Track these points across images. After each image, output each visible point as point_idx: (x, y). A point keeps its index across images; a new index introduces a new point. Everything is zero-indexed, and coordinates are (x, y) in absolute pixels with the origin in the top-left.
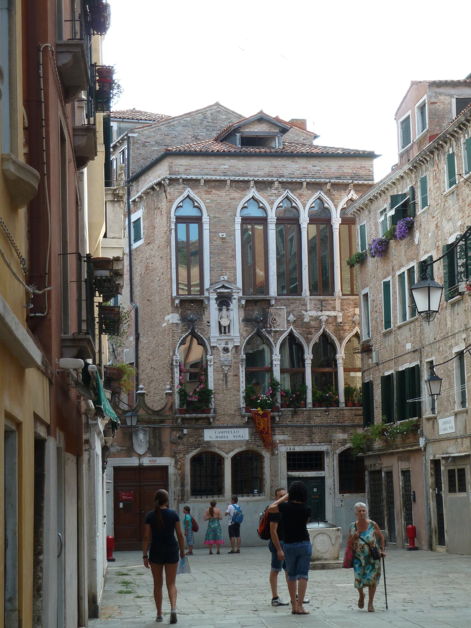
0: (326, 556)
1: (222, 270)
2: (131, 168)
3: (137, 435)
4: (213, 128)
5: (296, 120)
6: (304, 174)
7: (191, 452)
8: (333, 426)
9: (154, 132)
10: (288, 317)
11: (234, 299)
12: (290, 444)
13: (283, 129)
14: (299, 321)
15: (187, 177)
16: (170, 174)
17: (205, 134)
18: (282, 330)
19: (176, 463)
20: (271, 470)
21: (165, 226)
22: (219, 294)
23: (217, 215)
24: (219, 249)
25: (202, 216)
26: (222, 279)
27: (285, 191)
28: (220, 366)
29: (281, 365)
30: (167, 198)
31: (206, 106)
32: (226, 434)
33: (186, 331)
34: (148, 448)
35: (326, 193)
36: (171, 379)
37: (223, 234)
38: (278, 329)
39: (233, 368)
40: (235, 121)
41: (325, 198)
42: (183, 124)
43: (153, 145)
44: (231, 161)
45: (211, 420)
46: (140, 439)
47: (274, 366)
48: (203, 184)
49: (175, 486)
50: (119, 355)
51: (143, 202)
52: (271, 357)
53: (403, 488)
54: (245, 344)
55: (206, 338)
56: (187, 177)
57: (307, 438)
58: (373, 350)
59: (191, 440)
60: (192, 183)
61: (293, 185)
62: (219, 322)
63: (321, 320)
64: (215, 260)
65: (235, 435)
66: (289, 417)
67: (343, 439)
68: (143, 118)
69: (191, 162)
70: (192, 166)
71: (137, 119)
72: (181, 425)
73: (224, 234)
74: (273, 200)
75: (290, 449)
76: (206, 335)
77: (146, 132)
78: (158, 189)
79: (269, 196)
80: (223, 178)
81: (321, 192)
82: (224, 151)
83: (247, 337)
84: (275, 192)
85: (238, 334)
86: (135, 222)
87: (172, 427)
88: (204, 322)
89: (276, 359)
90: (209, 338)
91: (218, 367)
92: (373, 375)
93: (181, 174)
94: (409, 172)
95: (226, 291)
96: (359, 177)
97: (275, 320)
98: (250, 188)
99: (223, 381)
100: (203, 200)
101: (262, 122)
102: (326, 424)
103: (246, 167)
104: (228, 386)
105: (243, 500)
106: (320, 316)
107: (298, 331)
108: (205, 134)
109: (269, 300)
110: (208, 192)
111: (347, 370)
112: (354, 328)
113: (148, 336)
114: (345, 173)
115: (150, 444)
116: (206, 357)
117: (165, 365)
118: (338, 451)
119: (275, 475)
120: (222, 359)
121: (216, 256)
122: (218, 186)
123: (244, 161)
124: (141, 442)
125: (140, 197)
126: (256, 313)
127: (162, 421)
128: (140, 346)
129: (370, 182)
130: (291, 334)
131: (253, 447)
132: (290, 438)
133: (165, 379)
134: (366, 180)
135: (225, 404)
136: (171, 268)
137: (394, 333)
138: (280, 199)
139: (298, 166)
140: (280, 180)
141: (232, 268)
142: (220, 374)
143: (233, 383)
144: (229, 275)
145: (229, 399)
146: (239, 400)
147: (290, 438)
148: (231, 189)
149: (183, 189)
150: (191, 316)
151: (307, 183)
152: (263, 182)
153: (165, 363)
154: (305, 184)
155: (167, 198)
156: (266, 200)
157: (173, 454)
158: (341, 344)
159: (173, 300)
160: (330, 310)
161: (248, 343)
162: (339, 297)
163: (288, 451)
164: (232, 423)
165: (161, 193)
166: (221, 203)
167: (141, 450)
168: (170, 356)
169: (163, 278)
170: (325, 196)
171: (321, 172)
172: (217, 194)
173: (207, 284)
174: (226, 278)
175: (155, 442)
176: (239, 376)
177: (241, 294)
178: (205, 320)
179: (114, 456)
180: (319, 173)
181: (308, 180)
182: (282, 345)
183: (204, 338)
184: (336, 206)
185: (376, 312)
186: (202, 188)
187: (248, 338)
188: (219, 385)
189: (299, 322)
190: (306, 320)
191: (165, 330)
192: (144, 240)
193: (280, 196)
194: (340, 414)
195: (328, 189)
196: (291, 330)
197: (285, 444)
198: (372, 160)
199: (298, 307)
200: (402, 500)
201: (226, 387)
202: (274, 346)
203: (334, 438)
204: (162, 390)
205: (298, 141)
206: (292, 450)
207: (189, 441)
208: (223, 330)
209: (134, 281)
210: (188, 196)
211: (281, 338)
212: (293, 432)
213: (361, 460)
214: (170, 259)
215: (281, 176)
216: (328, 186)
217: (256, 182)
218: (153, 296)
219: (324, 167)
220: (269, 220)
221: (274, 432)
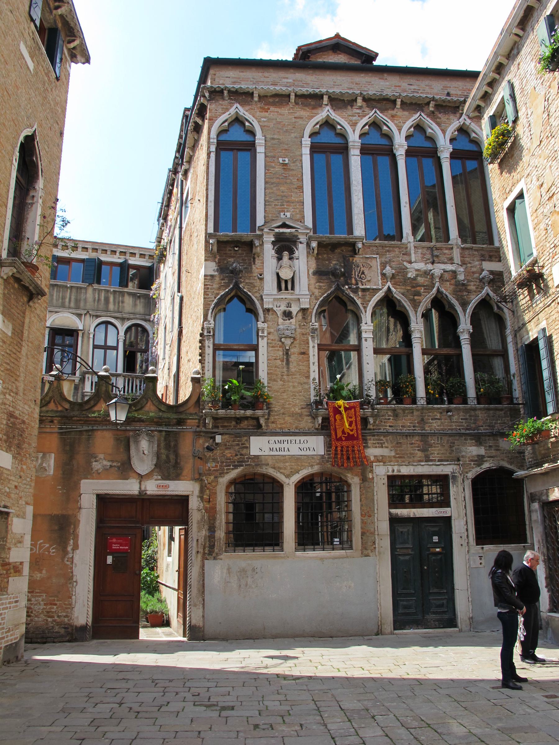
1: (283, 205)
3: (137, 442)
7: (227, 473)
8: (461, 435)
12: (392, 463)
14: (399, 277)
18: (375, 287)
19: (202, 491)
20: (362, 505)
23: (276, 137)
24: (277, 178)
27: (372, 110)
32: (286, 445)
33: (227, 286)
34: (155, 465)
35: (428, 116)
38: (368, 287)
39: (298, 341)
41: (428, 121)
44: (297, 74)
45: (262, 421)
46: (141, 449)
47: (363, 340)
49: (199, 530)
55: (256, 297)
57: (419, 454)
62: (278, 274)
64: (271, 191)
65: (302, 446)
66: (389, 419)
67: (478, 456)
69: (241, 74)
72: (212, 429)
74: (356, 120)
75: (393, 471)
76: (256, 292)
79: (350, 116)
81: (422, 114)
83: (321, 297)
84: (358, 111)
87: (196, 432)
90: (262, 296)
91: (275, 340)
95: (288, 230)
97: (363, 273)
98: (323, 106)
99: (283, 361)
100: (256, 119)
102: (450, 432)
104: (291, 371)
105: (314, 555)
106: (431, 270)
107: (398, 290)
110: (263, 110)
112: (483, 288)
115: (158, 458)
118: (471, 475)
120: (281, 327)
122: (277, 102)
126: (334, 263)
127: (180, 422)
132: (393, 454)
135: (285, 397)
141: (298, 203)
142: (278, 350)
143: (298, 365)
144: (293, 211)
145: (291, 389)
146: (308, 390)
147: (393, 454)
148: (297, 106)
150: (234, 265)
156: (346, 121)
157: (197, 476)
158: (465, 311)
160: (446, 263)
163: (390, 473)
164: (296, 428)
166: (283, 122)
170: (428, 119)
171: (420, 92)
172: (277, 112)
173: (260, 221)
175: (167, 456)
176: (308, 354)
178: (255, 270)
179: (99, 475)
187: (322, 298)
189: (400, 278)
193: (365, 116)
194: (470, 416)
195: (431, 111)
196: (389, 286)
197: (384, 463)
199: (398, 257)
201: (288, 371)
202: (363, 311)
203: (463, 453)
206: (396, 473)
208: (282, 284)
212: (397, 443)
216: (431, 105)
221: (366, 443)
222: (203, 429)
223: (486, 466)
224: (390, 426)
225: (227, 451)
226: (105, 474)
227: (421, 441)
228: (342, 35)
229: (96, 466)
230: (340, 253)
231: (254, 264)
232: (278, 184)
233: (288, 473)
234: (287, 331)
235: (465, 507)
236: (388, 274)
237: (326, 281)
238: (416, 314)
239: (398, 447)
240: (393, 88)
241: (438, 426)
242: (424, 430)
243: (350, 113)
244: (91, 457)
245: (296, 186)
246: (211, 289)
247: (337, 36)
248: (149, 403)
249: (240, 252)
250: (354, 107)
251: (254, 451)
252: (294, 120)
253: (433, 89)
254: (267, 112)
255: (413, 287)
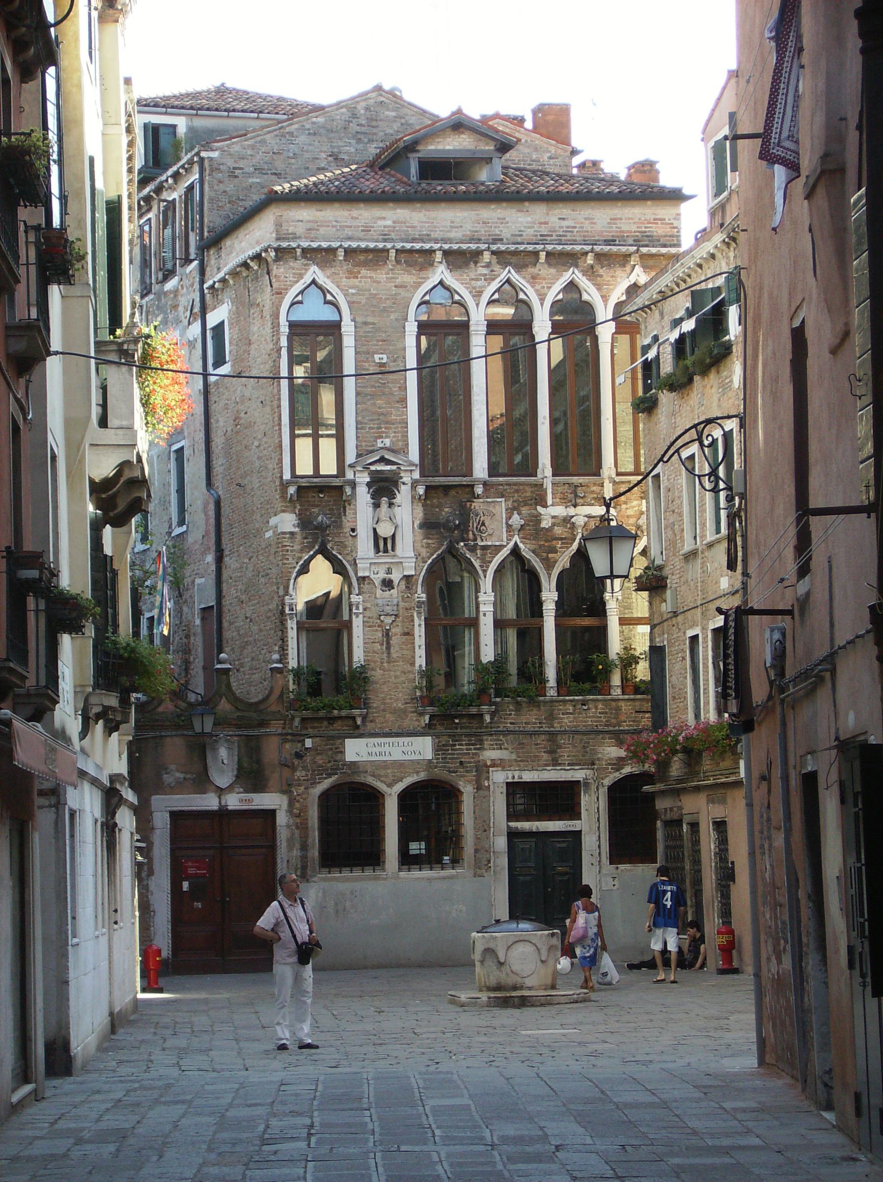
0: (529, 982)
1: (381, 428)
2: (206, 220)
3: (215, 750)
4: (370, 137)
5: (548, 105)
6: (541, 235)
9: (253, 147)
10: (509, 518)
11: (404, 484)
12: (512, 768)
13: (502, 143)
14: (532, 528)
15: (312, 244)
16: (278, 239)
17: (353, 150)
18: (497, 544)
20: (476, 818)
21: (269, 340)
22: (372, 474)
23: (370, 319)
24: (373, 386)
25: (341, 320)
26: (380, 445)
27: (504, 269)
28: (375, 616)
29: (495, 613)
30: (271, 286)
31: (354, 92)
32: (387, 749)
36: (280, 642)
37: (381, 356)
38: (489, 543)
40: (416, 122)
41: (583, 282)
42: (309, 129)
43: (249, 175)
44: (398, 211)
45: (359, 721)
47: (481, 614)
48: (341, 258)
49: (290, 848)
50: (188, 590)
51: (228, 290)
52: (477, 598)
53: (716, 854)
54: (424, 571)
56: (312, 244)
57: (545, 756)
58: (669, 585)
59: (320, 760)
60: (321, 256)
61: (520, 258)
62: (375, 530)
63: (573, 524)
65: (405, 749)
66: (511, 714)
68: (238, 107)
70: (322, 221)
71: (225, 111)
73: (384, 356)
74: (480, 287)
75: (513, 777)
76: (348, 554)
77: (236, 148)
78: (256, 268)
79: (473, 279)
80: (381, 245)
81: (576, 271)
82: (383, 192)
84: (485, 271)
85: (410, 554)
86: (213, 329)
88: (345, 531)
89: (486, 601)
90: (355, 560)
91: (372, 618)
92: (668, 634)
93: (300, 237)
94: (724, 248)
95: (388, 468)
96: (652, 241)
97: (483, 524)
98: (435, 264)
100: (342, 290)
101: (461, 130)
103: (428, 223)
106: (573, 517)
107: (528, 546)
108: (353, 150)
109: (472, 486)
111: (623, 621)
113: (238, 556)
114: (623, 232)
116: (349, 598)
117: (270, 614)
118: (607, 782)
119: (484, 826)
120: (380, 602)
121: (369, 400)
122: (371, 261)
123: (423, 212)
124: (224, 762)
125: (223, 281)
127: (262, 724)
128: (225, 576)
129: (673, 250)
130: (515, 551)
131: (440, 773)
132: (514, 756)
133: (270, 640)
134: (665, 246)
136: (280, 425)
137: (700, 556)
138: (495, 285)
139: (529, 219)
140: (494, 247)
143: (402, 649)
145: (393, 679)
147: (514, 756)
149: (302, 269)
150: (320, 518)
151: (547, 252)
152: (460, 253)
153: (270, 610)
154: (543, 255)
155: (271, 286)
157: (285, 787)
159: (284, 486)
161: (430, 570)
162: (610, 478)
165: (262, 275)
167: (223, 779)
168: (279, 597)
169: (266, 442)
170: (584, 279)
172: (371, 277)
174: (387, 442)
176: (413, 635)
177: (416, 475)
178: (347, 527)
179: (172, 790)
180: (572, 232)
181: (550, 248)
182: (499, 571)
183: (344, 562)
184: (605, 299)
185: (673, 512)
186: (341, 266)
187: (430, 561)
188: (374, 652)
190: (545, 524)
191: (270, 545)
192: (232, 366)
193: (494, 279)
196: (516, 543)
198: (679, 205)
200: (714, 877)
203: (600, 756)
204: (264, 662)
205: (539, 161)
207: (315, 762)
208: (383, 544)
209: (213, 444)
210: (314, 282)
211: (495, 559)
213: (650, 798)
214: (279, 406)
215: (496, 241)
217: (447, 253)
218: (249, 478)
219: (583, 220)
220: (471, 328)
222: (290, 731)
223: (627, 770)
224: (511, 723)
225: (318, 757)
226: (178, 788)
227: (549, 740)
228: (465, 111)
229: (168, 779)
230: (454, 497)
231: (345, 515)
232: (373, 396)
233: (390, 781)
234: (388, 608)
235: (598, 820)
236: (515, 526)
237: (436, 536)
238: (549, 577)
239: (520, 749)
240: (536, 227)
241: (570, 722)
242: (553, 727)
243: (472, 275)
244: (162, 768)
245: (397, 398)
246: (292, 551)
247: (459, 111)
248: (224, 700)
249: (326, 498)
250: (479, 265)
251: (350, 756)
252: (394, 291)
253: (595, 223)
254: (357, 277)
255: (546, 541)
